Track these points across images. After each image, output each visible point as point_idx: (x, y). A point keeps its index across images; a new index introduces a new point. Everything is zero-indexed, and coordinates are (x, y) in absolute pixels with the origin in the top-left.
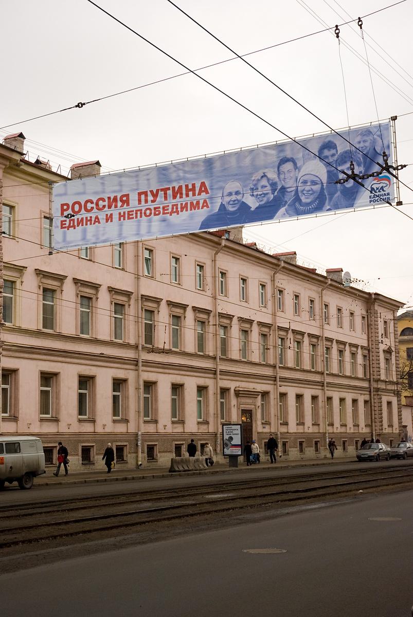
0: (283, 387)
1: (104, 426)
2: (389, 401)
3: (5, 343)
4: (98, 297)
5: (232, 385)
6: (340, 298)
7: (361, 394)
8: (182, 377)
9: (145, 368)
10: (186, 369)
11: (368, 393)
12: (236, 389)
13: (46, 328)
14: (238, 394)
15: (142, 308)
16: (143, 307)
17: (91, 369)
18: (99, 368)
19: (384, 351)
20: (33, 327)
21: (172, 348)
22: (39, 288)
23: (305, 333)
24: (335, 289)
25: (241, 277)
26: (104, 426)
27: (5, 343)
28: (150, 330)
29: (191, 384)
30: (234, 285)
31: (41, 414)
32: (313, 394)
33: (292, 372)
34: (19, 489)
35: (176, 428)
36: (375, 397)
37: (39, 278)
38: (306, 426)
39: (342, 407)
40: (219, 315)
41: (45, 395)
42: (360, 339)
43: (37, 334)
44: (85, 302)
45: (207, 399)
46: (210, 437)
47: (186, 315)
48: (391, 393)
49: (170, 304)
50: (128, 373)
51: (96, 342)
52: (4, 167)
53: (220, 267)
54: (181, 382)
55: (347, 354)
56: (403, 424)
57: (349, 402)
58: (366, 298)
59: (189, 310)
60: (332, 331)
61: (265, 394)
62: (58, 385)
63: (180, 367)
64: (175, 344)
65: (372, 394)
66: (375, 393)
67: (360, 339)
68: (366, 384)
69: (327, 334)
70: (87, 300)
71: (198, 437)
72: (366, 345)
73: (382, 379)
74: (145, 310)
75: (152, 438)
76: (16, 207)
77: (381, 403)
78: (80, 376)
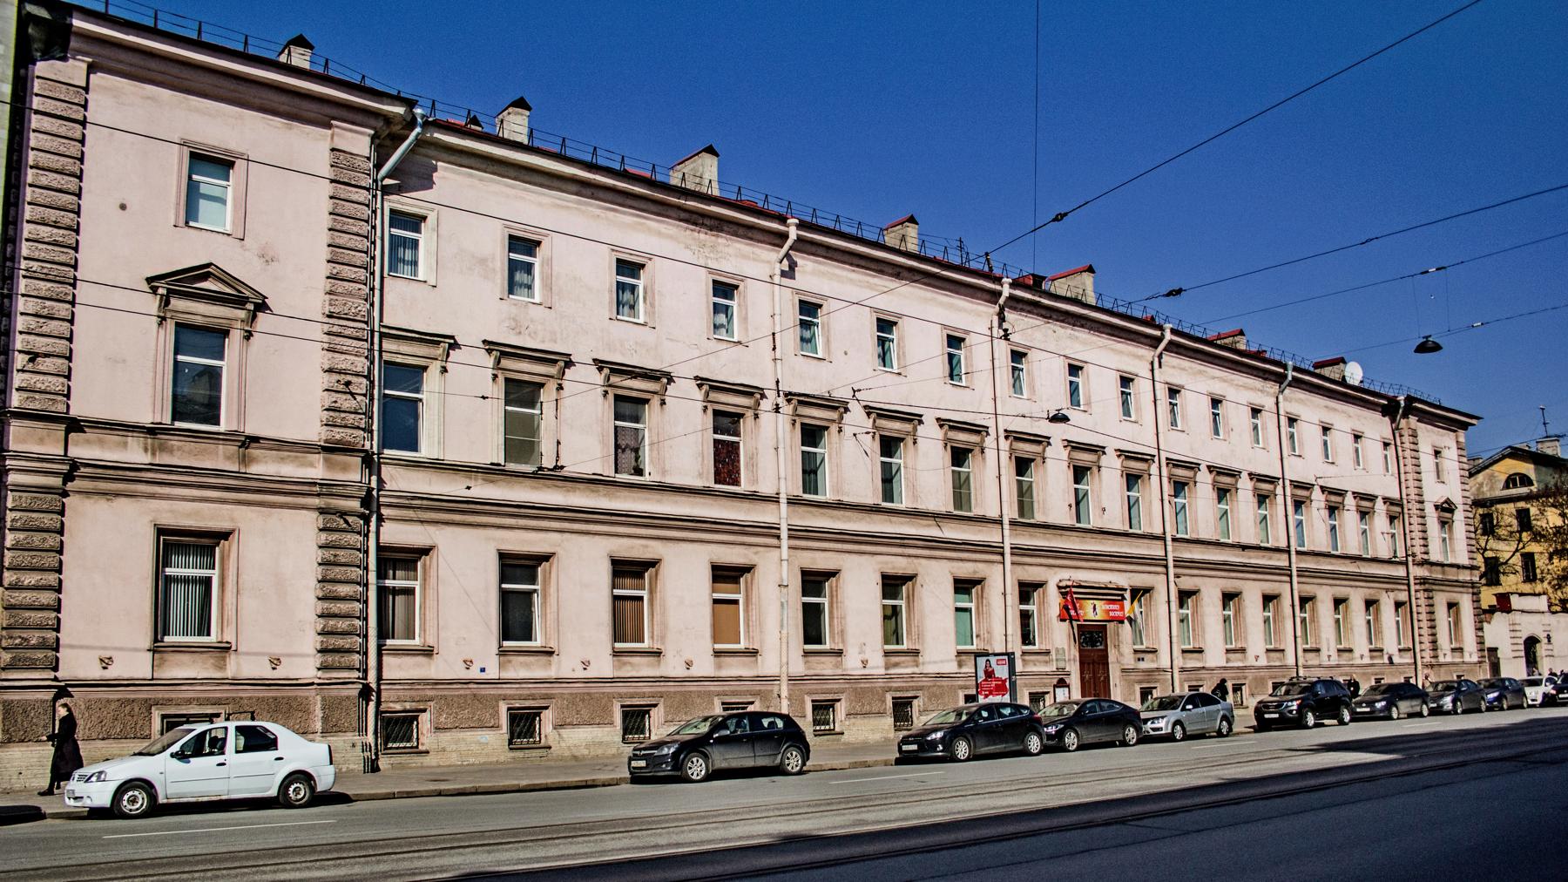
0: (1183, 578)
6: (1326, 407)
7: (1387, 590)
8: (910, 560)
11: (1406, 587)
12: (1061, 584)
13: (961, 509)
17: (647, 546)
18: (670, 544)
22: (793, 425)
24: (1233, 366)
26: (1257, 658)
28: (1024, 496)
30: (1309, 433)
32: (1368, 597)
33: (894, 519)
35: (896, 665)
36: (1419, 595)
37: (1009, 442)
39: (1345, 618)
40: (1167, 464)
41: (891, 615)
42: (1384, 485)
43: (492, 472)
45: (1277, 612)
46: (847, 686)
48: (1403, 584)
49: (1356, 495)
50: (756, 553)
51: (753, 497)
54: (1276, 592)
58: (1383, 406)
59: (1379, 502)
62: (981, 597)
63: (902, 541)
64: (888, 495)
65: (1413, 588)
66: (1418, 587)
71: (960, 683)
72: (1396, 495)
75: (828, 686)
76: (741, 288)
77: (1432, 605)
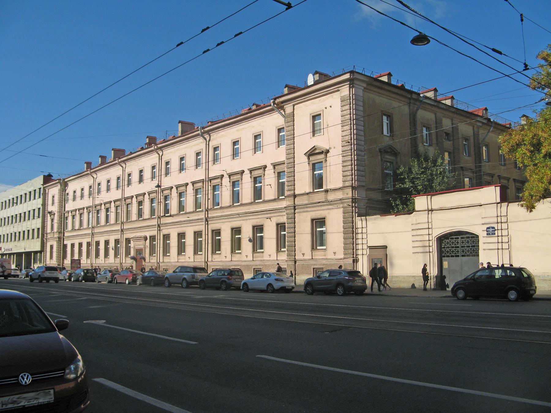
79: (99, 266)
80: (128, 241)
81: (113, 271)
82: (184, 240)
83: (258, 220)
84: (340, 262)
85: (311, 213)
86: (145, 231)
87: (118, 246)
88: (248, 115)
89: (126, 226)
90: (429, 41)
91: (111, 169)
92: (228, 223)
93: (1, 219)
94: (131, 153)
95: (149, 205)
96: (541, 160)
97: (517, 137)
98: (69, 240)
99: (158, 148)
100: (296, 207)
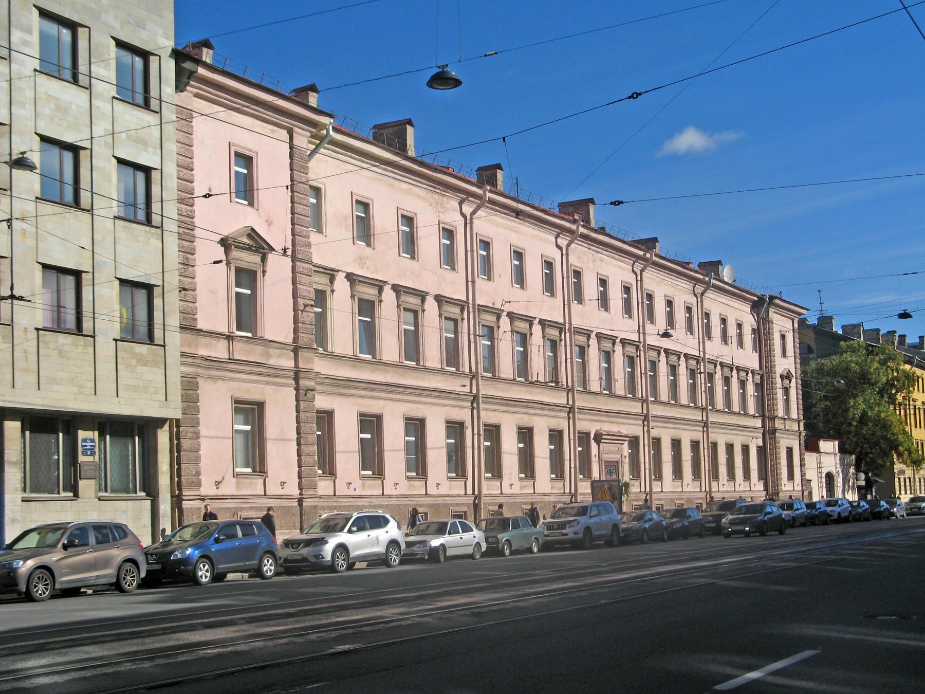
1: (283, 484)
2: (729, 442)
3: (320, 376)
4: (334, 288)
5: (592, 428)
8: (530, 416)
9: (582, 416)
10: (535, 405)
14: (598, 438)
15: (479, 323)
16: (480, 321)
19: (782, 377)
20: (349, 352)
21: (358, 353)
23: (386, 282)
25: (722, 316)
27: (320, 376)
29: (541, 427)
31: (449, 472)
34: (758, 536)
38: (506, 482)
40: (479, 310)
44: (245, 279)
47: (500, 324)
52: (309, 134)
53: (573, 263)
55: (663, 368)
56: (808, 477)
57: (738, 450)
60: (714, 349)
61: (634, 442)
67: (749, 359)
68: (636, 408)
69: (577, 322)
70: (367, 307)
73: (780, 415)
74: (482, 325)
78: (362, 415)
79: (752, 498)
80: (583, 438)
81: (689, 513)
82: (363, 436)
83: (526, 417)
84: (439, 500)
85: (235, 384)
86: (620, 423)
87: (580, 449)
88: (744, 294)
89: (486, 389)
90: (700, 265)
91: (526, 226)
92: (723, 435)
93: (923, 392)
94: (601, 231)
95: (614, 366)
96: (879, 433)
97: (859, 412)
98: (510, 412)
99: (644, 257)
100: (301, 375)
